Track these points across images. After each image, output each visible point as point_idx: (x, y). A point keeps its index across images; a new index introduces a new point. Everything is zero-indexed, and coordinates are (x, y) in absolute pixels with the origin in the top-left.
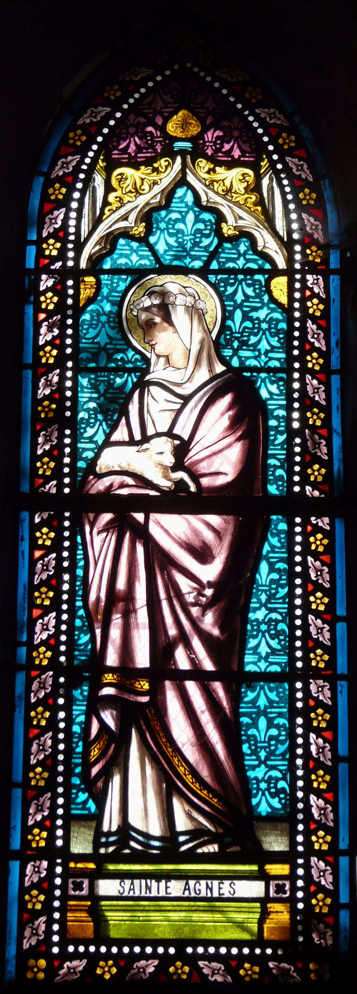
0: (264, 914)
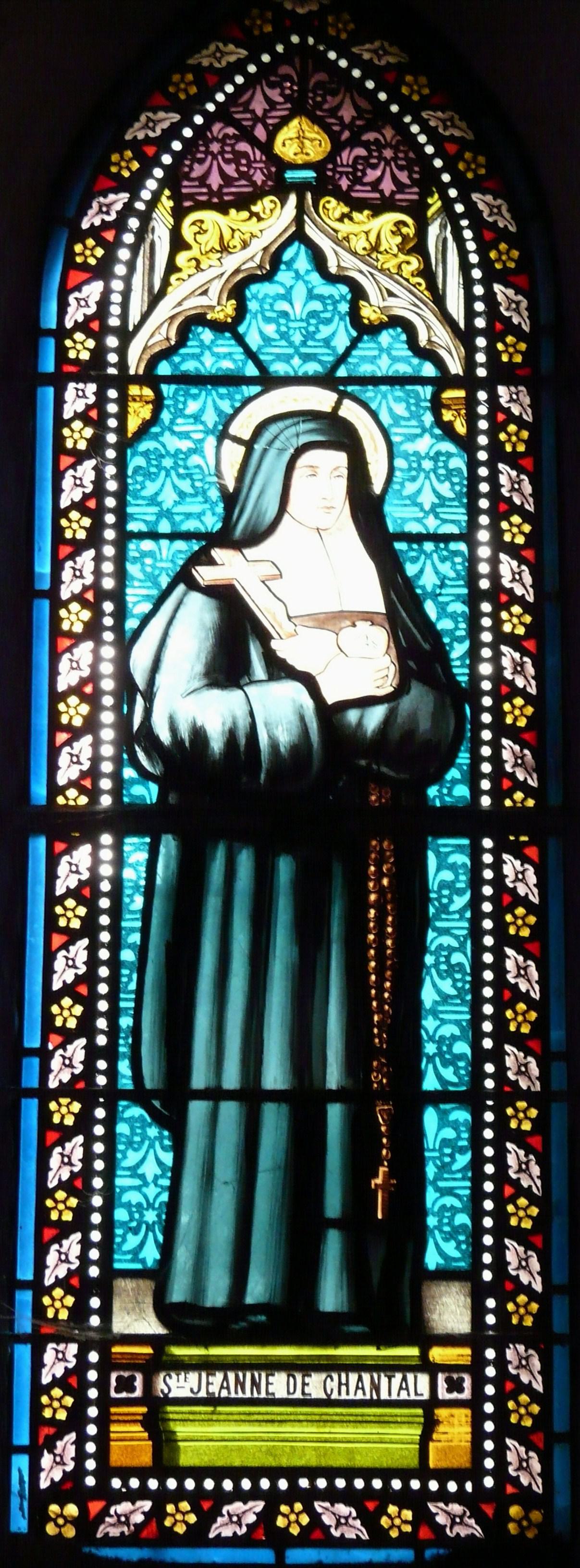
0: (430, 1425)
